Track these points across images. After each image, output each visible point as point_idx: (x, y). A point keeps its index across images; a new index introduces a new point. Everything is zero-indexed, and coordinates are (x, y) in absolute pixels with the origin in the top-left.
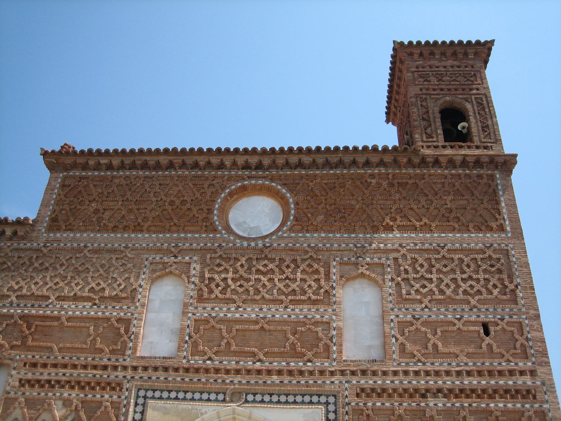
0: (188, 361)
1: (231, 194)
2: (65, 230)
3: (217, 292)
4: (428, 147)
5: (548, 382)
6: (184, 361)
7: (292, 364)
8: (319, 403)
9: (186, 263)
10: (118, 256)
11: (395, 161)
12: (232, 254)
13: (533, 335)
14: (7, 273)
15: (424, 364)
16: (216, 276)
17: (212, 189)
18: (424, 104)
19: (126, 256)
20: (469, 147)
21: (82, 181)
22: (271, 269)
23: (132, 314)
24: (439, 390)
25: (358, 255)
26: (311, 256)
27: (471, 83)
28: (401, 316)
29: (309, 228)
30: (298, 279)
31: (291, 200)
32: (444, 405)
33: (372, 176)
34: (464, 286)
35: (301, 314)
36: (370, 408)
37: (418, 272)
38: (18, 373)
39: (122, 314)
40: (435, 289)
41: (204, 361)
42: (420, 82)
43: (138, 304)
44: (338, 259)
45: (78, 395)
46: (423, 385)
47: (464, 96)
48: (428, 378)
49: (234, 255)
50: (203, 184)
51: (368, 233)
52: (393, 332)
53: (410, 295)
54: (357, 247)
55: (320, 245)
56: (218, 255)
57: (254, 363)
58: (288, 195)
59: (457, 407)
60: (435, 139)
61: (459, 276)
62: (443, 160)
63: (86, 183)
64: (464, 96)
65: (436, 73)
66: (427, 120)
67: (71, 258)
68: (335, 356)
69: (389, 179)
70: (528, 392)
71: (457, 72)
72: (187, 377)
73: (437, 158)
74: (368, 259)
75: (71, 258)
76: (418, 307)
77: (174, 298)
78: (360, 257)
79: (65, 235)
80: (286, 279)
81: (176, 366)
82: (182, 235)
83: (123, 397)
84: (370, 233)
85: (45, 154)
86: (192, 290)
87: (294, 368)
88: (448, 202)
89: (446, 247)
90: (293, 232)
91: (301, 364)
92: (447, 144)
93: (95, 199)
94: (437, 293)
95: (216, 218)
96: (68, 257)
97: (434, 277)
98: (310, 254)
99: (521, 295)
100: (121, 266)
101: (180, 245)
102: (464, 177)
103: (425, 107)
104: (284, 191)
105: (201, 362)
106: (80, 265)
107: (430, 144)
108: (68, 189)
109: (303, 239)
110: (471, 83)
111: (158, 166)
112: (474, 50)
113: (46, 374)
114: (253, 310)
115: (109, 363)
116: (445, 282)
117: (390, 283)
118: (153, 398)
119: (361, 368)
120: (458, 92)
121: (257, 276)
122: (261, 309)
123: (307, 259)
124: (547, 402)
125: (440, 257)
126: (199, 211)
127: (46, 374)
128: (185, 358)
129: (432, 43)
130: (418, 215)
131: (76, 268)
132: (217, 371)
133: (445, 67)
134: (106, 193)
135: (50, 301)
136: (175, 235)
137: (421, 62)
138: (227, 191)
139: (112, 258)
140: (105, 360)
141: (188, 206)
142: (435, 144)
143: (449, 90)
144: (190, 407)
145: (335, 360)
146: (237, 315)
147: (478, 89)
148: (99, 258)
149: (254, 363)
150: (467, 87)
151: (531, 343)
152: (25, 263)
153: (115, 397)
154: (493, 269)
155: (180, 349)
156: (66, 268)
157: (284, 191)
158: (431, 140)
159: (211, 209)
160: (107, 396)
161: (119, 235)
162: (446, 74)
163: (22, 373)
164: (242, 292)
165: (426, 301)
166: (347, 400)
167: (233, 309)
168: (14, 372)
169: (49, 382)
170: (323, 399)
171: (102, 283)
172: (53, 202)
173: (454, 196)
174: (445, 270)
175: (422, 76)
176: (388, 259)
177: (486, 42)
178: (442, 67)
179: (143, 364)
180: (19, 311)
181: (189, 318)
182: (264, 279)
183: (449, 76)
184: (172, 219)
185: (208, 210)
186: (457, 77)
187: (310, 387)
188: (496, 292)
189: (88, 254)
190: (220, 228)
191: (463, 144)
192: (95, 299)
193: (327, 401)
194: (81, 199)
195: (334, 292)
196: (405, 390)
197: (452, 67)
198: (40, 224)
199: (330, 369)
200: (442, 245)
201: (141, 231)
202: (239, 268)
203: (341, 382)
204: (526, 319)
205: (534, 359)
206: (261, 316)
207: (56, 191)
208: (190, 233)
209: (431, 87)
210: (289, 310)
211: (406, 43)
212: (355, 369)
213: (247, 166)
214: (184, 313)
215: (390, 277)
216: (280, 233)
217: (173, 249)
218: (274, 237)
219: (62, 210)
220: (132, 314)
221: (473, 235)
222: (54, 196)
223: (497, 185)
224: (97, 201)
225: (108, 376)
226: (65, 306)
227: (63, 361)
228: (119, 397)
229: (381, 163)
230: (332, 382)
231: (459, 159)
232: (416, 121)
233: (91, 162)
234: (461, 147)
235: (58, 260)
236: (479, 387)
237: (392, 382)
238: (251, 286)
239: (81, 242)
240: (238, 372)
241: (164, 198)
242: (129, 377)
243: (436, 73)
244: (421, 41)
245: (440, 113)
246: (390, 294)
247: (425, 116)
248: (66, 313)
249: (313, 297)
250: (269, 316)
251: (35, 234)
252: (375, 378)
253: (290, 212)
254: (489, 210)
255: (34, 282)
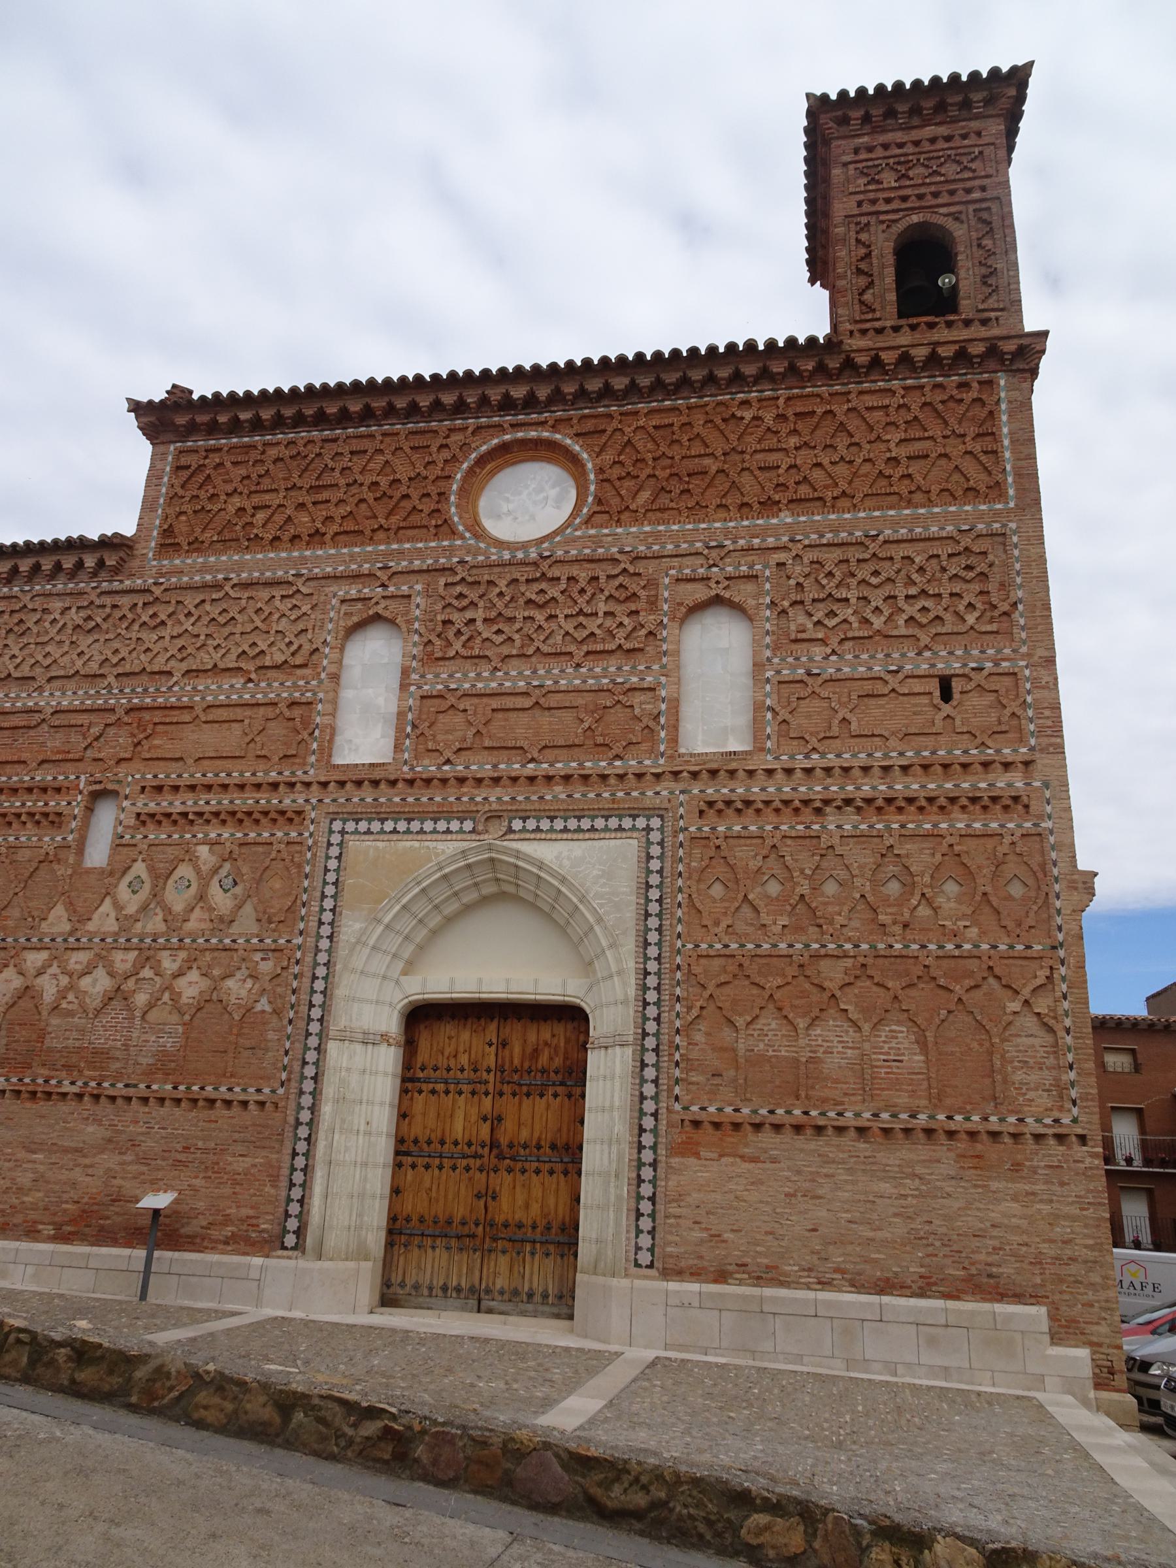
0: (412, 769)
1: (481, 461)
2: (188, 551)
3: (458, 645)
4: (864, 332)
5: (1054, 783)
6: (406, 769)
7: (588, 764)
8: (634, 828)
9: (403, 596)
10: (284, 593)
11: (792, 369)
12: (483, 575)
13: (1037, 696)
14: (96, 637)
15: (823, 755)
16: (455, 617)
17: (446, 454)
18: (864, 237)
19: (298, 591)
20: (949, 324)
21: (211, 456)
22: (553, 598)
23: (315, 694)
24: (848, 802)
25: (711, 562)
26: (625, 570)
27: (971, 175)
28: (784, 672)
29: (622, 517)
30: (601, 614)
31: (590, 466)
32: (855, 827)
33: (745, 403)
34: (911, 610)
35: (605, 677)
36: (722, 835)
37: (823, 587)
38: (133, 804)
39: (297, 694)
40: (852, 619)
41: (439, 768)
42: (859, 186)
43: (323, 675)
44: (672, 572)
45: (232, 835)
46: (819, 792)
47: (953, 209)
48: (829, 781)
49: (486, 577)
50: (428, 447)
51: (731, 520)
52: (768, 702)
53: (804, 631)
54: (708, 548)
55: (642, 548)
56: (458, 578)
57: (523, 766)
58: (585, 456)
59: (879, 830)
60: (878, 315)
61: (901, 591)
62: (888, 357)
63: (217, 460)
64: (953, 209)
65: (896, 160)
66: (866, 274)
67: (203, 601)
68: (662, 748)
69: (778, 407)
70: (1016, 799)
71: (941, 154)
72: (410, 795)
73: (877, 355)
74: (729, 569)
75: (203, 601)
76: (818, 652)
77: (386, 660)
78: (715, 565)
79: (189, 561)
80: (578, 614)
81: (392, 777)
82: (395, 546)
83: (307, 834)
84: (736, 519)
85: (136, 407)
86: (415, 644)
87: (590, 772)
88: (892, 445)
89: (881, 538)
90: (592, 527)
91: (603, 764)
92: (903, 322)
93: (235, 490)
94: (855, 625)
95: (453, 510)
96: (197, 601)
97: (852, 595)
98: (623, 566)
99: (1022, 622)
100: (291, 610)
101: (391, 564)
102: (931, 390)
103: (864, 244)
104: (577, 448)
105: (433, 768)
106: (220, 614)
107: (868, 325)
108: (185, 474)
109: (610, 539)
110: (971, 175)
111: (344, 418)
112: (985, 93)
113: (177, 803)
114: (520, 673)
115: (280, 778)
116: (874, 604)
117: (768, 613)
118: (356, 832)
119: (708, 766)
120: (940, 201)
121: (526, 614)
122: (535, 672)
123: (617, 576)
124: (1050, 817)
125: (867, 556)
126: (424, 500)
127: (177, 803)
128: (406, 762)
129: (890, 89)
130: (830, 475)
131: (213, 619)
132: (461, 780)
133: (917, 143)
134: (254, 476)
135: (175, 679)
136: (382, 547)
137: (866, 139)
138: (473, 456)
139: (273, 597)
140: (273, 774)
141: (403, 490)
142: (877, 324)
143: (920, 197)
144: (417, 844)
145: (662, 755)
146: (494, 685)
147: (983, 189)
148: (252, 598)
149: (523, 766)
150: (960, 185)
151: (1030, 713)
152: (124, 616)
153: (294, 834)
154: (971, 575)
155: (398, 748)
156: (196, 621)
157: (577, 448)
158: (870, 316)
159: (444, 493)
160: (280, 834)
161: (284, 555)
162: (918, 160)
163: (140, 804)
164: (502, 643)
165: (834, 642)
166: (681, 823)
167: (486, 674)
168: (126, 803)
169: (185, 815)
170: (641, 823)
171: (259, 643)
172: (162, 501)
173: (906, 431)
174: (874, 581)
175: (865, 171)
176: (765, 567)
177: (1014, 70)
178: (909, 145)
179: (337, 778)
180: (124, 701)
181: (411, 695)
182: (540, 616)
183: (923, 165)
184: (375, 517)
185: (440, 494)
186: (942, 164)
187: (619, 802)
188: (971, 619)
189: (231, 593)
190: (461, 528)
191: (937, 320)
192: (249, 672)
193: (648, 825)
194: (211, 491)
195: (665, 633)
196: (786, 803)
197: (933, 140)
198: (143, 544)
199: (653, 771)
200: (873, 533)
201: (323, 544)
202: (496, 600)
203: (672, 793)
204: (1027, 667)
205: (1033, 742)
206: (536, 683)
207: (166, 479)
208: (408, 541)
209: (881, 195)
210: (583, 670)
211: (834, 97)
212: (697, 768)
213: (507, 404)
214: (404, 686)
215: (768, 600)
216: (569, 530)
217: (379, 573)
218: (558, 539)
219: (181, 513)
220: (315, 694)
221: (936, 510)
222: (164, 490)
223: (998, 402)
224: (241, 493)
225: (280, 802)
226: (200, 688)
227: (205, 781)
228: (301, 834)
229: (764, 375)
230: (657, 793)
231: (920, 353)
232: (844, 277)
233: (222, 419)
234: (931, 326)
235: (180, 607)
236: (923, 794)
237: (763, 789)
238: (517, 631)
239: (218, 571)
240: (496, 780)
241: (360, 478)
242: (314, 801)
243: (896, 160)
244: (867, 86)
245: (895, 254)
246: (768, 633)
247: (863, 266)
248: (203, 698)
249: (627, 646)
250: (549, 683)
251: (136, 563)
252: (732, 784)
253: (587, 488)
254: (975, 457)
255: (143, 648)
